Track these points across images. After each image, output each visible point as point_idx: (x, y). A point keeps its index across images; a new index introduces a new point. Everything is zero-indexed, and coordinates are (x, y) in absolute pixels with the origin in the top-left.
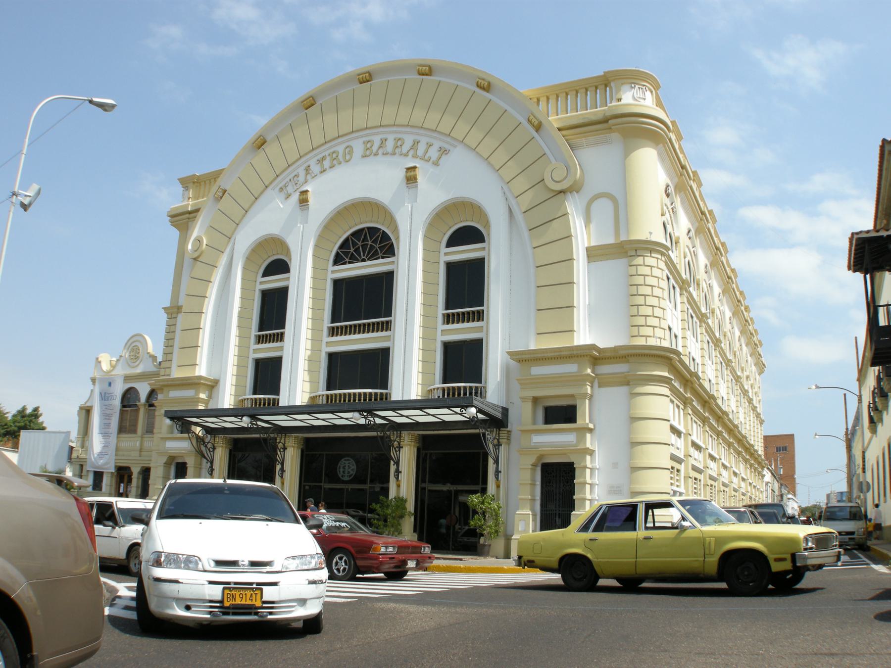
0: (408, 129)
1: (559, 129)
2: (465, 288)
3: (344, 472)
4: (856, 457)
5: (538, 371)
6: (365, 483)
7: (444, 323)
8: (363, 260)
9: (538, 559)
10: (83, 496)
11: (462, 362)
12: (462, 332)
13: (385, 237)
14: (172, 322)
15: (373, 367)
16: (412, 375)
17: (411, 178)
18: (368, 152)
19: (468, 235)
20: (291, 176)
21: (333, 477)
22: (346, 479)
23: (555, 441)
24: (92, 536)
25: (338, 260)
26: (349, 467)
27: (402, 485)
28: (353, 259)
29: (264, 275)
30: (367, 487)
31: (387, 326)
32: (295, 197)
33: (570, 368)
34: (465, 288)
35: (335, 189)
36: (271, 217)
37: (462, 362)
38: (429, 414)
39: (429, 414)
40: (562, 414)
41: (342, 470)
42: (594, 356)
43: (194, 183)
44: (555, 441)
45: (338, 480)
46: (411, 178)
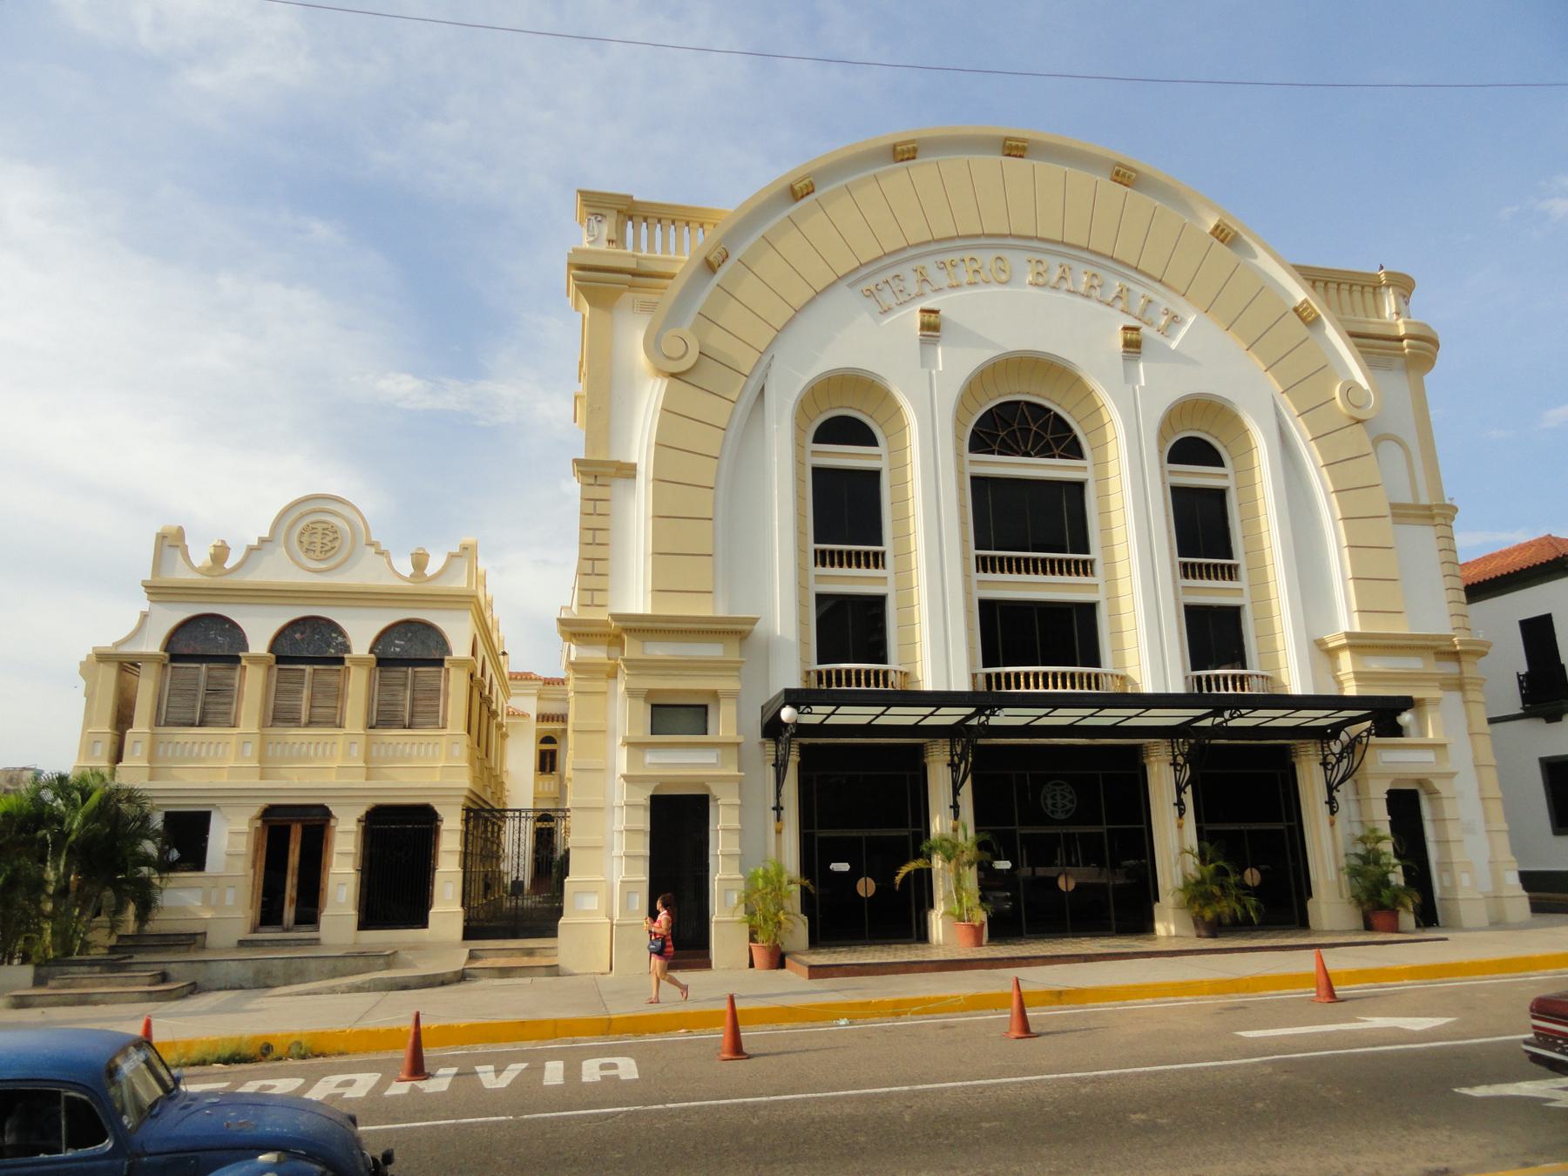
2: (1203, 528)
3: (1054, 805)
6: (1101, 823)
8: (1027, 454)
9: (210, 1058)
10: (279, 1162)
11: (1215, 635)
12: (851, 581)
13: (1061, 425)
14: (598, 492)
15: (1070, 633)
16: (1144, 651)
18: (1041, 280)
22: (1060, 816)
24: (1176, 356)
26: (1064, 797)
27: (785, 832)
28: (1007, 450)
30: (1103, 829)
31: (877, 560)
32: (913, 318)
33: (1414, 664)
34: (1203, 528)
36: (866, 340)
37: (1215, 635)
38: (956, 792)
39: (956, 792)
41: (1049, 802)
43: (619, 212)
45: (1046, 820)
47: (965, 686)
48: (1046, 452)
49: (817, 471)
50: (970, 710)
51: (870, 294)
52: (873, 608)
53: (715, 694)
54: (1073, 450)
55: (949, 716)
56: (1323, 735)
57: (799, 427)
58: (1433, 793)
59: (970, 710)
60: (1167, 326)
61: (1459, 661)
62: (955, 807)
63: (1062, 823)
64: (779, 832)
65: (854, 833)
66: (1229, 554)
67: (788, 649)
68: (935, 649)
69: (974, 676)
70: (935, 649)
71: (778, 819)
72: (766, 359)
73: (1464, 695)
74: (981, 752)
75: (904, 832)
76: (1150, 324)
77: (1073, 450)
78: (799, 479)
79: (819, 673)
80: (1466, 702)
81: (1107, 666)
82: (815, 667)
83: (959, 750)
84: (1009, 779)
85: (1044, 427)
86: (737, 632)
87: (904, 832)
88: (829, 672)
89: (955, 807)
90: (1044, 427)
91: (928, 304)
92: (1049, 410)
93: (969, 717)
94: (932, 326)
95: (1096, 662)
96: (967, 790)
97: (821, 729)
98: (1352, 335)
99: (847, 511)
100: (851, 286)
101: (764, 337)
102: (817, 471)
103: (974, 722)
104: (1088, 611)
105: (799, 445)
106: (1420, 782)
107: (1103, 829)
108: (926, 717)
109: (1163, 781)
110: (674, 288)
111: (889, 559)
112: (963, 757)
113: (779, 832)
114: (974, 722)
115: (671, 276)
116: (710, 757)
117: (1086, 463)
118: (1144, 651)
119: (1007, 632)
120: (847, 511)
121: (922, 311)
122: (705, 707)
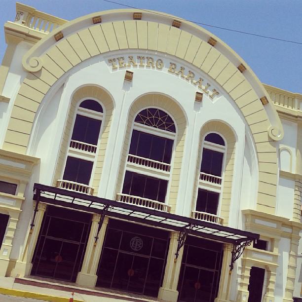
0: (199, 71)
1: (277, 111)
2: (212, 164)
3: (134, 245)
4: (168, 276)
5: (258, 221)
7: (128, 161)
11: (207, 201)
12: (210, 186)
15: (157, 189)
16: (181, 201)
17: (199, 98)
19: (214, 138)
20: (120, 56)
21: (126, 246)
23: (259, 258)
25: (138, 119)
27: (33, 235)
29: (81, 106)
30: (149, 257)
31: (94, 150)
32: (122, 73)
34: (212, 164)
35: (153, 81)
36: (103, 76)
37: (207, 201)
38: (178, 250)
39: (178, 250)
40: (261, 245)
42: (284, 223)
44: (259, 258)
45: (131, 250)
46: (199, 98)
47: (188, 216)
48: (162, 127)
49: (134, 131)
50: (187, 224)
51: (110, 61)
52: (215, 197)
53: (19, 181)
54: (173, 129)
55: (180, 224)
56: (236, 243)
57: (130, 115)
58: (269, 271)
59: (187, 224)
60: (213, 95)
61: (292, 228)
62: (177, 254)
63: (135, 252)
64: (95, 246)
65: (60, 240)
66: (169, 163)
67: (49, 173)
68: (105, 183)
69: (192, 213)
70: (105, 183)
71: (231, 270)
72: (67, 74)
73: (291, 240)
74: (188, 237)
75: (78, 243)
76: (207, 93)
77: (173, 129)
78: (127, 132)
79: (196, 214)
80: (291, 243)
81: (91, 184)
82: (195, 211)
83: (182, 236)
84: (120, 232)
85: (157, 115)
86: (32, 163)
87: (78, 243)
88: (125, 197)
89: (177, 254)
90: (164, 119)
91: (130, 70)
92: (166, 114)
93: (187, 226)
94: (129, 77)
95: (163, 200)
96: (182, 249)
97: (54, 201)
98: (277, 111)
99: (86, 131)
100: (104, 57)
101: (68, 67)
102: (134, 131)
103: (188, 228)
104: (165, 183)
105: (129, 121)
106: (266, 266)
107: (149, 257)
108: (163, 220)
109: (174, 244)
110: (40, 43)
111: (172, 169)
112: (183, 239)
113: (95, 246)
114: (188, 228)
115: (39, 39)
116: (11, 203)
117: (226, 147)
118: (181, 201)
119: (135, 184)
120: (86, 131)
121: (127, 71)
122: (17, 185)
